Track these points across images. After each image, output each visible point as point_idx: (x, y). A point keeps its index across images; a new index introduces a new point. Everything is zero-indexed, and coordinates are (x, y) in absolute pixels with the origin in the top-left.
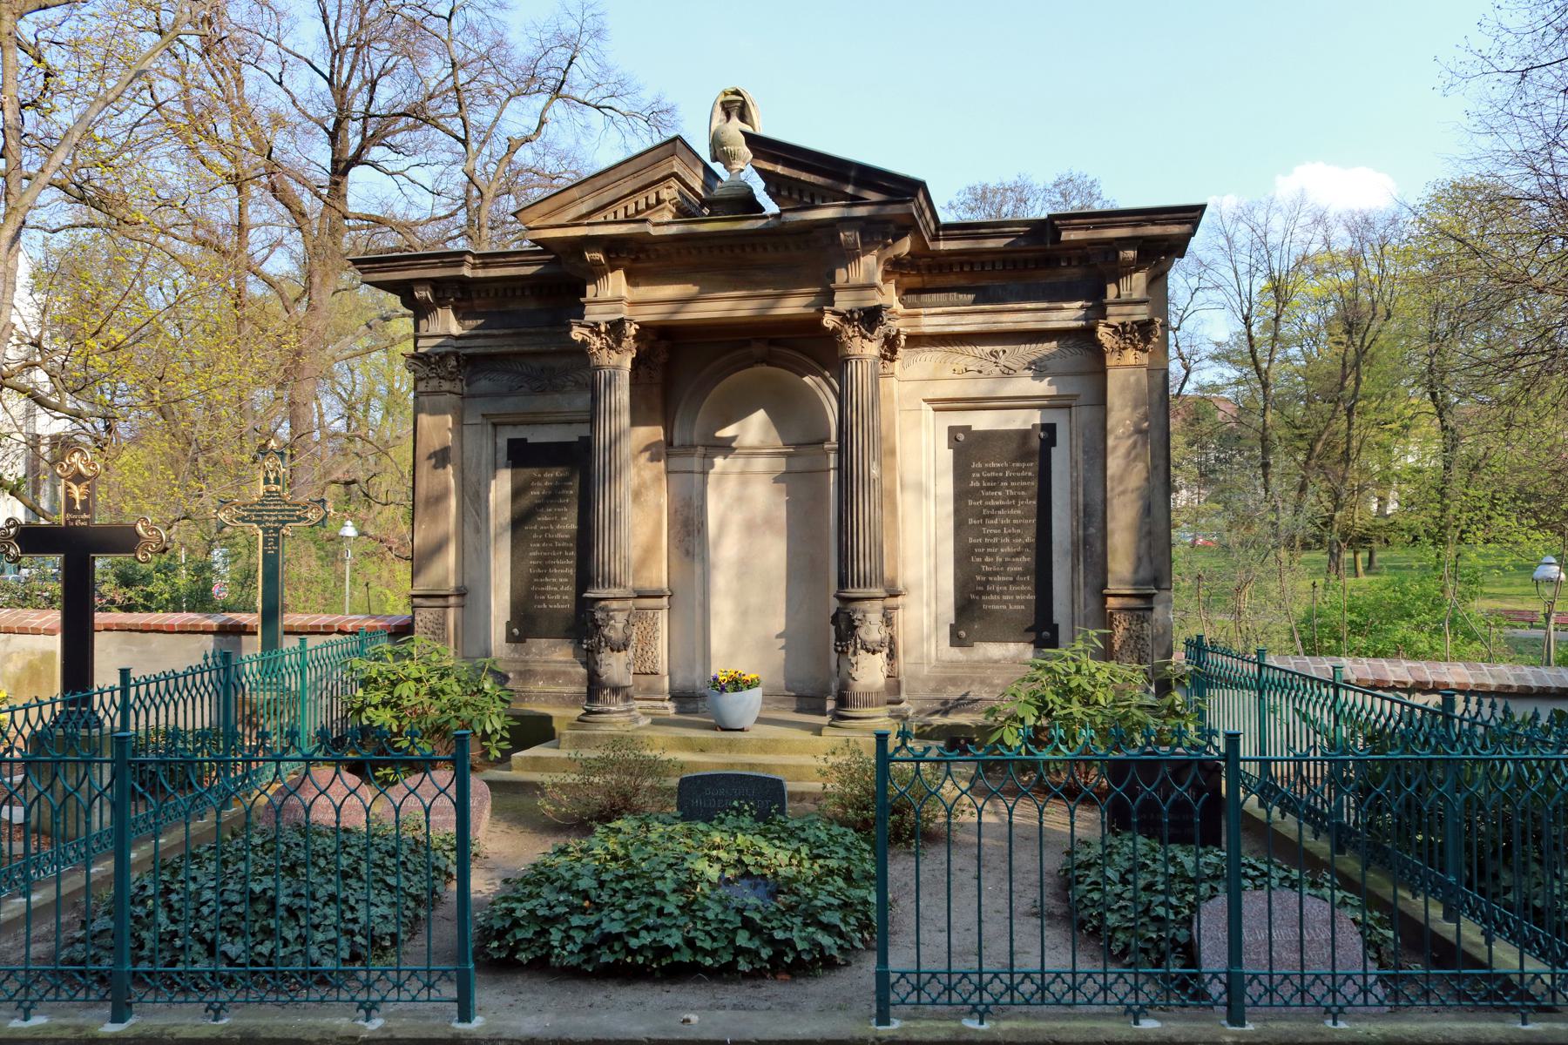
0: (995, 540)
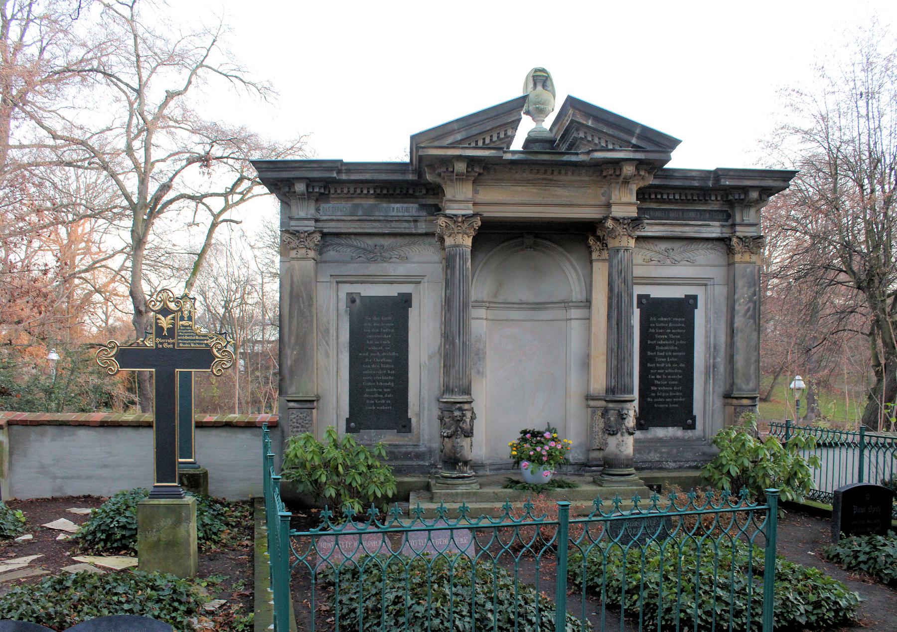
0: (663, 365)
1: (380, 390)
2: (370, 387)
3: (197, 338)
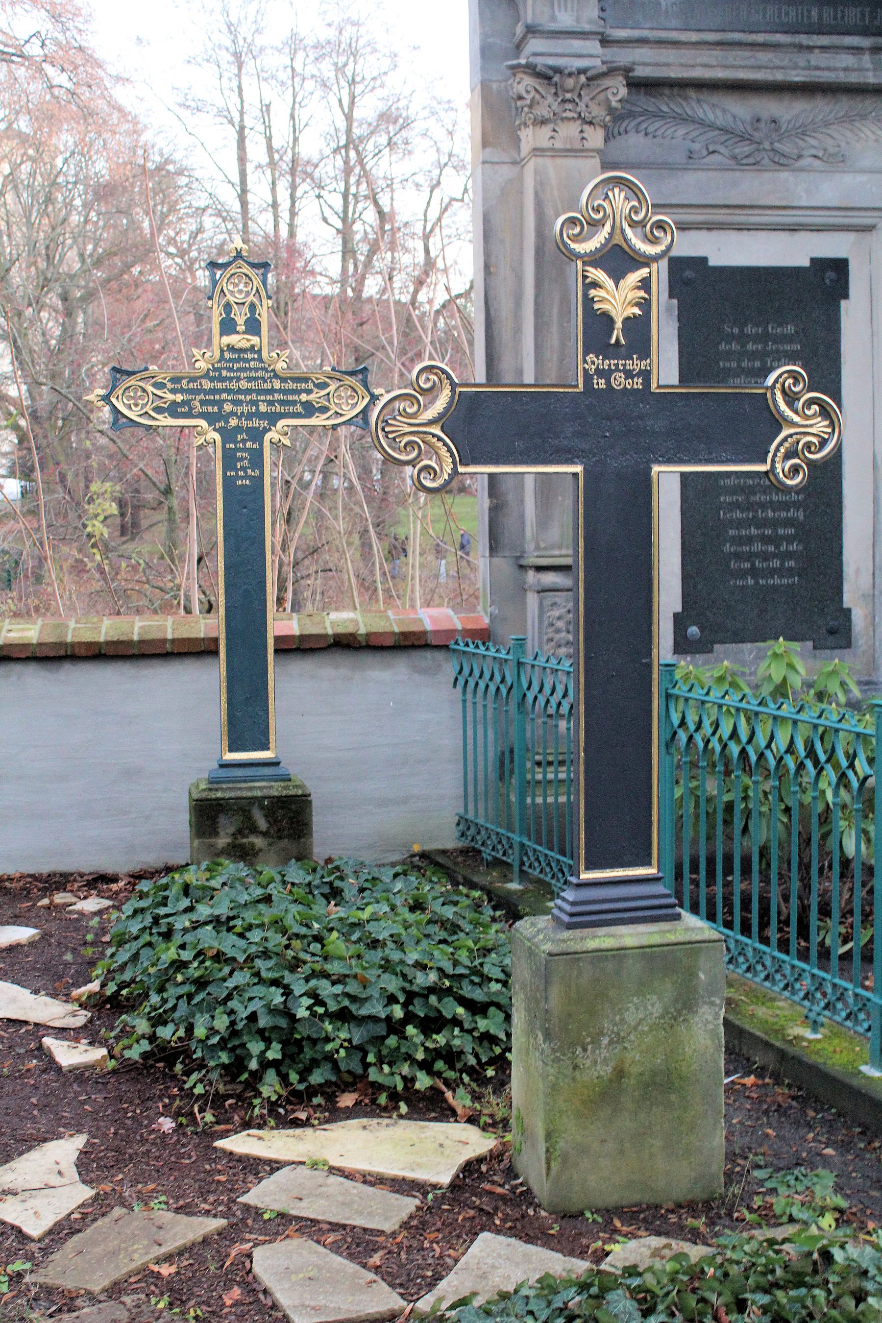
1: (768, 532)
2: (739, 524)
3: (277, 385)
